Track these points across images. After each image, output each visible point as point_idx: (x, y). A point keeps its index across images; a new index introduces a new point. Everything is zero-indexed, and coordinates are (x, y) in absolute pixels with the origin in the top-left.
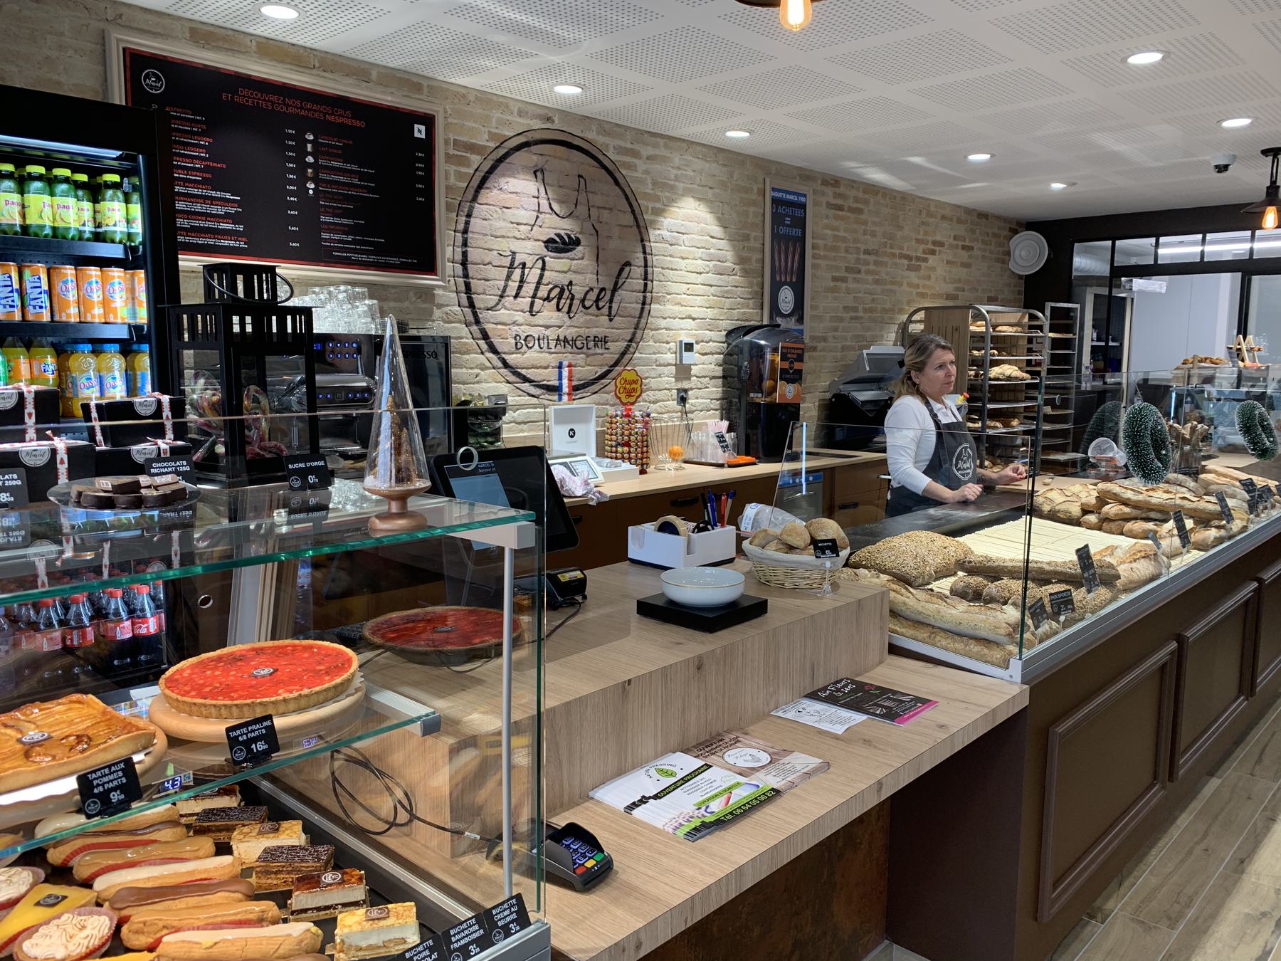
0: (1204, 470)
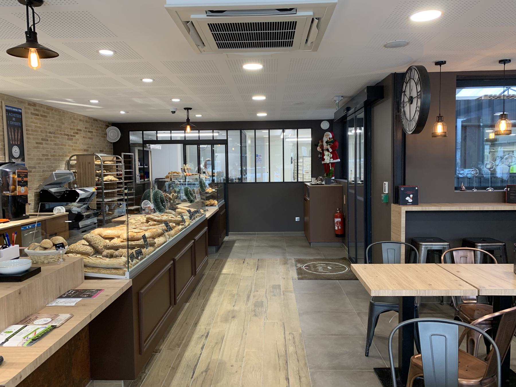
0: (177, 208)
